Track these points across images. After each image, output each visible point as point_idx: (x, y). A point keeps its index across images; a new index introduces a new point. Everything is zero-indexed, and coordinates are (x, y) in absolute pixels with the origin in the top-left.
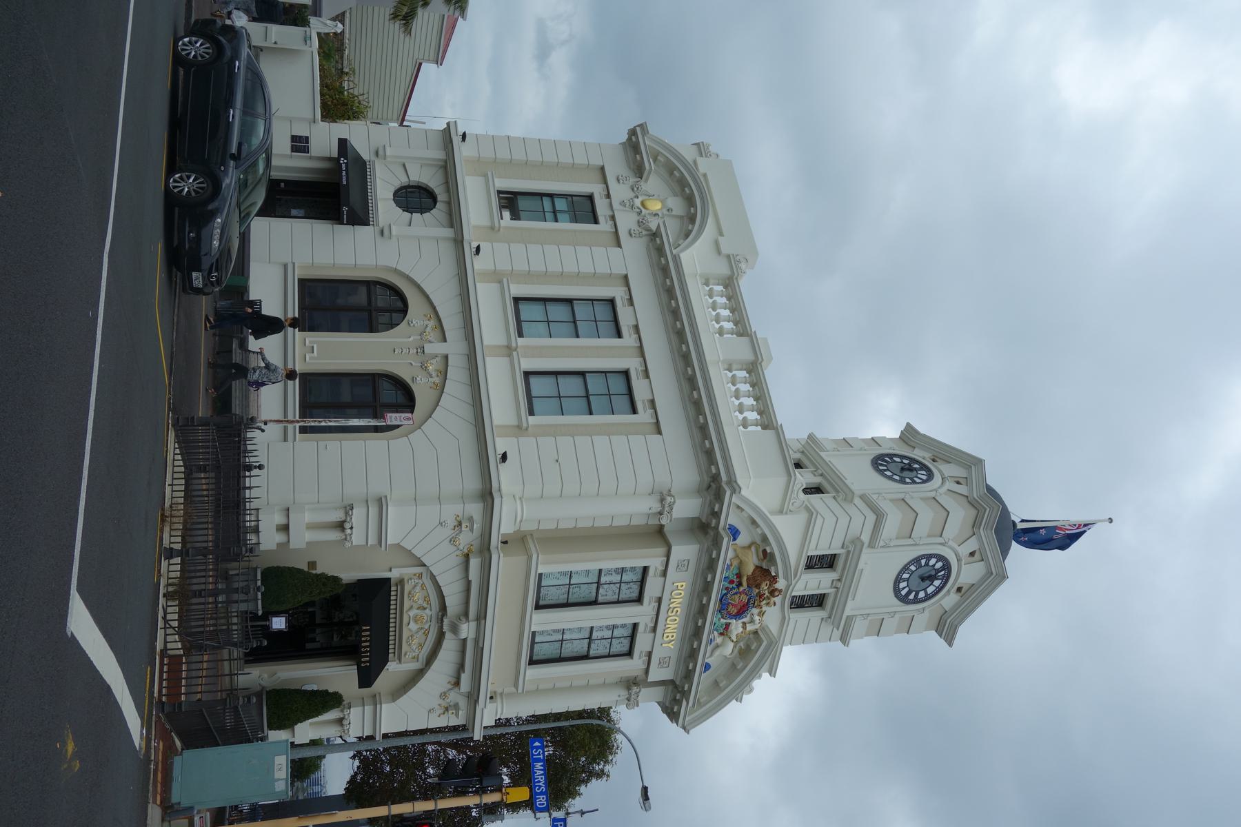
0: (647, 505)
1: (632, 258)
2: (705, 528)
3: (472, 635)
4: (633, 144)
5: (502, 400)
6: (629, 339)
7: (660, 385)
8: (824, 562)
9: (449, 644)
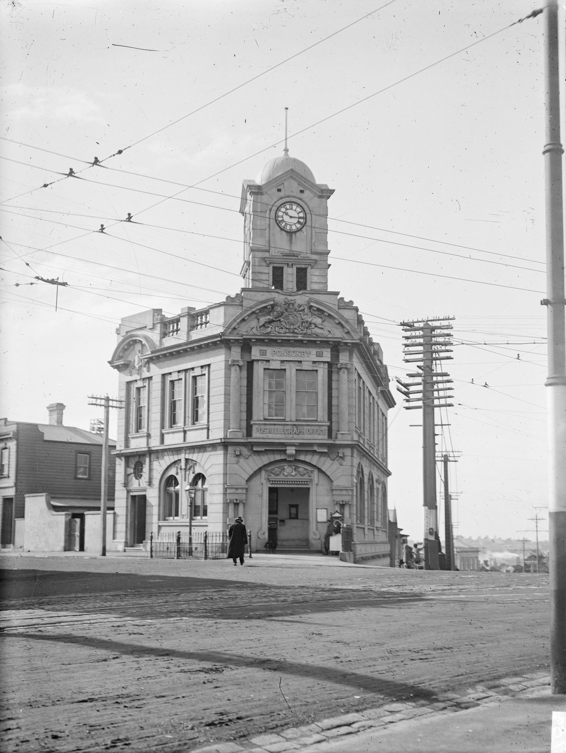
0: (234, 372)
1: (156, 371)
2: (246, 345)
3: (294, 448)
4: (117, 367)
5: (196, 437)
6: (182, 376)
7: (194, 362)
8: (278, 279)
9: (302, 457)
